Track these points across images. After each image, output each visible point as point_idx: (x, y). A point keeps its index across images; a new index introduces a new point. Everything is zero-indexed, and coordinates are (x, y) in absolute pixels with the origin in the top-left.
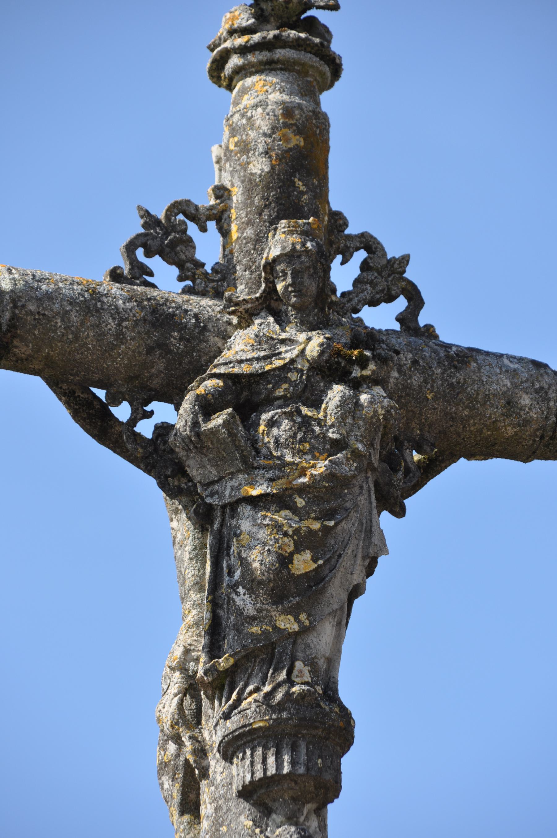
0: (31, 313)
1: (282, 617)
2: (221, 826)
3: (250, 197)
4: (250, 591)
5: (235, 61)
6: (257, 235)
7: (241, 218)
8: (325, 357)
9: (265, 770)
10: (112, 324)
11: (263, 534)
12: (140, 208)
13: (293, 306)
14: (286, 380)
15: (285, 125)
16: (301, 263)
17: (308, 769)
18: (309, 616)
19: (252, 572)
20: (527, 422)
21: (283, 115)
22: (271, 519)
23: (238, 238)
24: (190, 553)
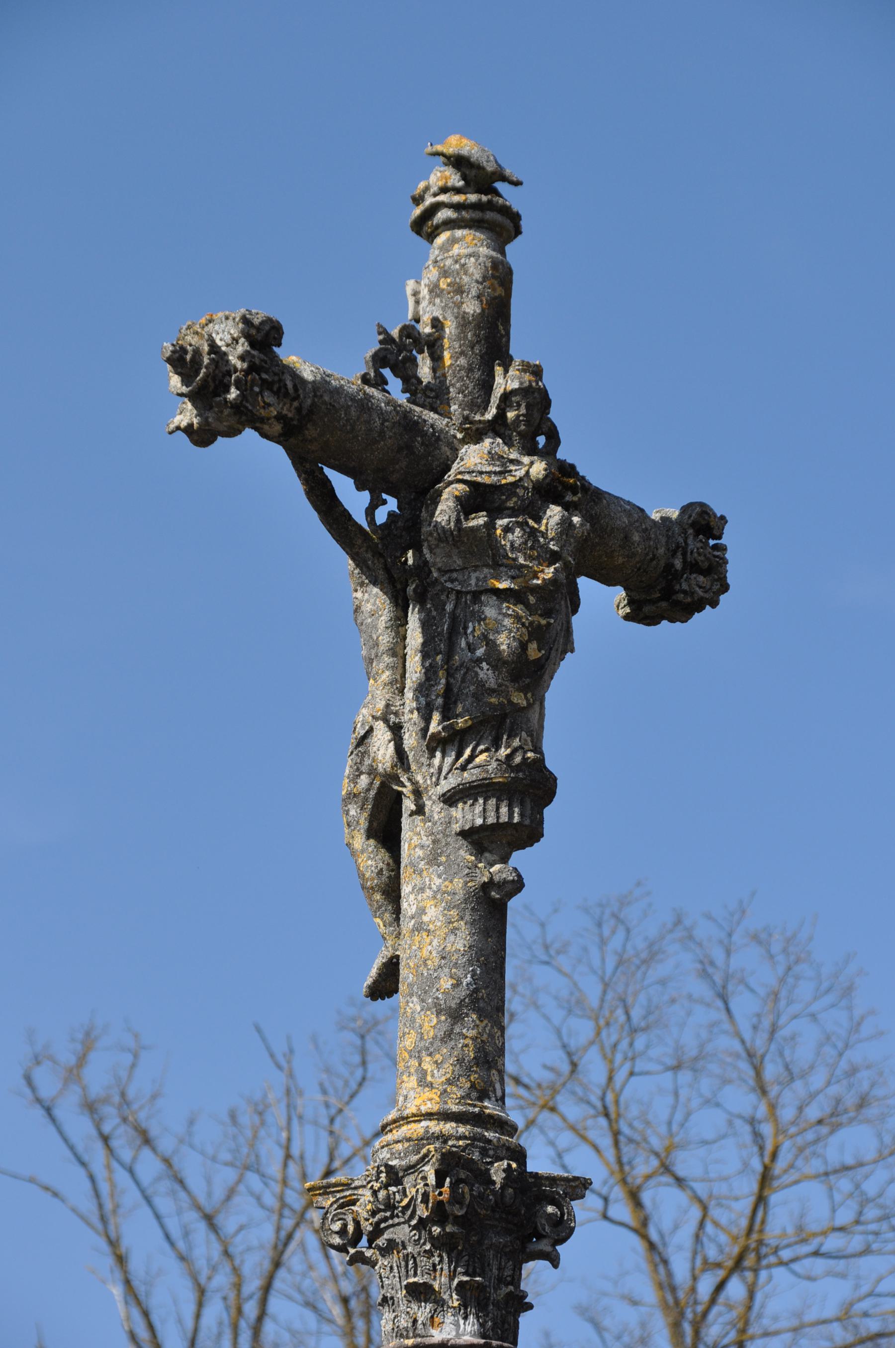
0: (325, 403)
1: (516, 694)
2: (440, 856)
3: (463, 332)
4: (494, 668)
5: (443, 215)
6: (470, 365)
7: (455, 348)
8: (548, 480)
9: (498, 818)
10: (378, 422)
11: (507, 622)
12: (379, 326)
13: (519, 434)
14: (515, 494)
15: (493, 276)
16: (535, 398)
17: (532, 821)
18: (533, 695)
19: (500, 652)
20: (634, 555)
21: (492, 267)
22: (514, 611)
23: (451, 365)
24: (386, 623)
